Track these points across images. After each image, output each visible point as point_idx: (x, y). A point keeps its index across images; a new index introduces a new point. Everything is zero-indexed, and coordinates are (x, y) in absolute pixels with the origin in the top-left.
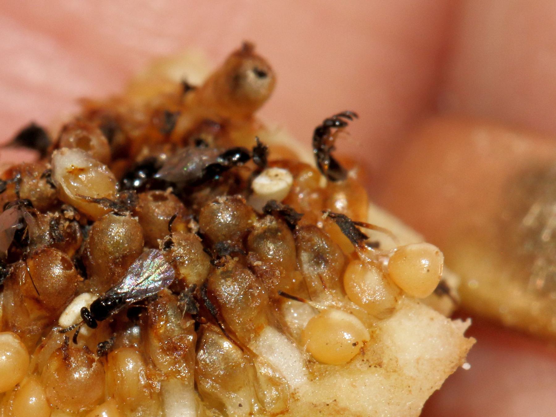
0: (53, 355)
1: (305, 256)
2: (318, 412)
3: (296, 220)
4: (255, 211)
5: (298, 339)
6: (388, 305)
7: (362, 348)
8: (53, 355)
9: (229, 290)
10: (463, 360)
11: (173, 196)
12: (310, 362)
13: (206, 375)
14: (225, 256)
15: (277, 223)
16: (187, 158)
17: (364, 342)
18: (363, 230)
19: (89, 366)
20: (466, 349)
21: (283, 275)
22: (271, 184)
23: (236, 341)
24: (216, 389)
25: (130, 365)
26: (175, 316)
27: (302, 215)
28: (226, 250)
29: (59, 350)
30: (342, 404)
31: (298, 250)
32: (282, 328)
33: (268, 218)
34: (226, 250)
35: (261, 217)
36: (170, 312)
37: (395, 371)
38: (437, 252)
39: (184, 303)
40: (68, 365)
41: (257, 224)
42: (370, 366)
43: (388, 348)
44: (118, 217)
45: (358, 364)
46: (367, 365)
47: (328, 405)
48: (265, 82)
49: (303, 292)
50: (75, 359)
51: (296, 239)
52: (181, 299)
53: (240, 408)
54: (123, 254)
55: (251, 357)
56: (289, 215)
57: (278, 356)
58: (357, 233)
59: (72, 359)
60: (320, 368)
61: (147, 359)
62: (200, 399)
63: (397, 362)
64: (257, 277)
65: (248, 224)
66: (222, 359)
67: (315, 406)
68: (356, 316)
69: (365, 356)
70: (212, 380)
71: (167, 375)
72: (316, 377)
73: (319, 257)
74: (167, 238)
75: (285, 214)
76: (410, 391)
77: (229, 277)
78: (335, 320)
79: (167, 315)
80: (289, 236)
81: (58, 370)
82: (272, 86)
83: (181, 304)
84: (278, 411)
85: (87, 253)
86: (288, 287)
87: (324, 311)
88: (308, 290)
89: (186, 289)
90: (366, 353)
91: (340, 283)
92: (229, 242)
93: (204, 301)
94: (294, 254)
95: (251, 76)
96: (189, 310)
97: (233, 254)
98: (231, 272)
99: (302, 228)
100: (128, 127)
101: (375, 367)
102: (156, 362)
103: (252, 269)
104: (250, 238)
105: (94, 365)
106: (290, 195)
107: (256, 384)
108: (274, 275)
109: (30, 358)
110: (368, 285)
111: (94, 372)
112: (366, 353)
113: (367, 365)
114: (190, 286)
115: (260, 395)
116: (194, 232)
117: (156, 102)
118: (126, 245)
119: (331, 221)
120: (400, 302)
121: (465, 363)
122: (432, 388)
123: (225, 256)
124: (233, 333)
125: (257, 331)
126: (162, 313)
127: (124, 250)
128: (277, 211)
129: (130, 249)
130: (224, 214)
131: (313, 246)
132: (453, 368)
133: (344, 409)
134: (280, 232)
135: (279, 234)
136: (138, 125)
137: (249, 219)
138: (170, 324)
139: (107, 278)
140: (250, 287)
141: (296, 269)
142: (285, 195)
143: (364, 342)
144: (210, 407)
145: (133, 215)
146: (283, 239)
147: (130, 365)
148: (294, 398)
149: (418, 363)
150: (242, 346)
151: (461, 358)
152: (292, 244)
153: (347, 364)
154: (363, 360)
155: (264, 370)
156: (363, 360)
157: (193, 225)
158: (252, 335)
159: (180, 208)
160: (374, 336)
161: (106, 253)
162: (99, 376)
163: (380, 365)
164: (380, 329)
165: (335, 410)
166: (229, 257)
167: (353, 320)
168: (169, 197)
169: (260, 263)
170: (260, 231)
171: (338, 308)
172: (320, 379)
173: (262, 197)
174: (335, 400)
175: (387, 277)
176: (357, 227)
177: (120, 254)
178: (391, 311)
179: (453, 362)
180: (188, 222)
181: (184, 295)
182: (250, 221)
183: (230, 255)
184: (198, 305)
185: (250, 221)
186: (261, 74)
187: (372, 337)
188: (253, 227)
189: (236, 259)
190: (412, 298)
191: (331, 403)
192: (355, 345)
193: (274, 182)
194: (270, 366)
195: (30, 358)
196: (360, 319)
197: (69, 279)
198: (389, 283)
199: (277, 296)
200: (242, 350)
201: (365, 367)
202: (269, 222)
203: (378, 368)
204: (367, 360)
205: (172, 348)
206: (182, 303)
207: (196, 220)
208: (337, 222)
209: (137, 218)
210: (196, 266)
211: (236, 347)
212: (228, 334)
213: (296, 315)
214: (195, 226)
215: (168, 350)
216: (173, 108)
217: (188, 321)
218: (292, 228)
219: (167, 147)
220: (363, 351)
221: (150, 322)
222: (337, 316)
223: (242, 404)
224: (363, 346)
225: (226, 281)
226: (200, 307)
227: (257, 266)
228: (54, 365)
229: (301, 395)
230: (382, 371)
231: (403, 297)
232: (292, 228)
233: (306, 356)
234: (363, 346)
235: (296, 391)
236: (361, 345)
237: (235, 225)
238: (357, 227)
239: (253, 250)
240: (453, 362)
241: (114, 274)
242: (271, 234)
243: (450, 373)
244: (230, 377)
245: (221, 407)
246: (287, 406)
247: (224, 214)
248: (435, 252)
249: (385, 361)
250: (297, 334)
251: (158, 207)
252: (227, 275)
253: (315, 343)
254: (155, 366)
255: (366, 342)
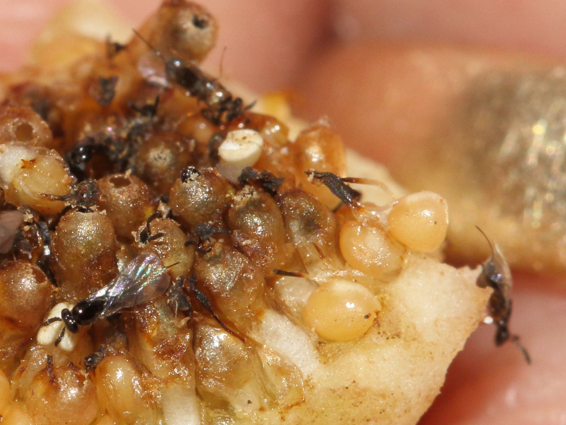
0: (36, 378)
1: (295, 226)
2: (338, 397)
3: (278, 187)
4: (230, 183)
5: (300, 320)
6: (394, 267)
7: (375, 319)
8: (36, 378)
9: (215, 275)
10: (484, 314)
11: (135, 177)
12: (321, 343)
13: (205, 375)
14: (208, 239)
15: (259, 193)
16: (124, 126)
17: (377, 313)
18: (354, 186)
19: (80, 385)
20: (484, 301)
21: (276, 251)
22: (239, 148)
23: (235, 332)
24: (220, 388)
25: (120, 373)
26: (167, 315)
27: (282, 180)
28: (208, 232)
29: (43, 371)
30: (363, 384)
31: (285, 220)
32: (279, 307)
33: (247, 189)
34: (208, 232)
35: (238, 188)
36: (159, 313)
37: (414, 339)
38: (441, 201)
39: (174, 299)
40: (57, 388)
41: (237, 198)
42: (388, 338)
43: (402, 314)
44: (85, 214)
45: (373, 337)
46: (384, 337)
47: (347, 388)
48: (207, 31)
49: (297, 267)
50: (62, 379)
51: (281, 208)
52: (171, 296)
53: (245, 403)
54: (97, 255)
55: (254, 347)
56: (270, 182)
57: (282, 340)
58: (347, 194)
59: (60, 380)
60: (332, 347)
61: (140, 368)
62: (199, 400)
63: (414, 328)
64: (249, 258)
65: (226, 198)
66: (222, 354)
67: (334, 391)
68: (361, 284)
69: (381, 328)
70: (215, 379)
71: (166, 382)
72: (329, 358)
73: (310, 225)
74: (142, 228)
75: (262, 180)
76: (432, 358)
77: (219, 262)
78: (339, 293)
79: (157, 315)
80: (275, 206)
81: (46, 395)
82: (214, 34)
83: (170, 302)
84: (293, 402)
85: (55, 259)
86: (283, 264)
87: (325, 284)
88: (302, 261)
89: (174, 284)
90: (379, 322)
91: (335, 249)
92: (210, 222)
93: (196, 293)
94: (282, 224)
95: (188, 25)
96: (180, 306)
97: (217, 236)
98: (219, 257)
99: (286, 194)
100: (60, 103)
101: (393, 338)
102: (151, 369)
103: (240, 249)
104: (231, 214)
105: (85, 383)
106: (262, 159)
107: (262, 376)
108: (267, 253)
109: (10, 384)
110: (365, 244)
111: (87, 390)
112: (379, 322)
113: (384, 337)
114: (177, 279)
115: (268, 386)
116: (164, 216)
117: (85, 69)
118: (100, 244)
119: (318, 182)
120: (406, 261)
121: (485, 317)
122: (454, 350)
123: (208, 239)
124: (232, 324)
125: (257, 316)
126: (151, 315)
127: (99, 250)
128: (257, 180)
129: (104, 248)
130: (197, 191)
131: (302, 212)
132: (474, 324)
133: (365, 390)
134: (264, 203)
135: (263, 205)
136: (70, 99)
137: (226, 193)
138: (160, 323)
139: (82, 283)
140: (244, 271)
141: (286, 241)
142: (257, 158)
143: (377, 313)
144: (213, 408)
145: (100, 209)
146: (268, 210)
147: (120, 373)
148: (308, 385)
149: (436, 325)
150: (241, 337)
151: (480, 312)
152: (278, 214)
153: (359, 338)
154: (379, 333)
155: (268, 359)
156: (379, 333)
157: (163, 208)
158: (254, 323)
159: (146, 191)
160: (385, 302)
161: (78, 256)
162: (90, 395)
163: (398, 335)
164: (390, 294)
165: (356, 393)
166: (213, 240)
167: (358, 288)
168: (131, 180)
169: (249, 242)
170: (242, 205)
171: (341, 278)
172: (334, 361)
173: (233, 165)
174: (354, 381)
175: (389, 237)
176: (346, 183)
177: (94, 256)
178: (398, 272)
179: (472, 318)
180: (156, 205)
181: (173, 291)
182: (227, 195)
183: (213, 237)
184: (188, 298)
185: (227, 195)
186: (199, 23)
187: (383, 305)
188: (233, 201)
189: (221, 241)
190: (417, 253)
191: (350, 385)
192: (367, 317)
193: (244, 146)
194: (275, 353)
195: (10, 384)
196: (366, 286)
197: (45, 292)
198: (392, 243)
199: (272, 273)
200: (243, 340)
201: (382, 340)
202: (248, 194)
203: (397, 339)
204: (384, 332)
205: (168, 351)
206: (172, 300)
207: (166, 201)
208: (324, 182)
209: (104, 212)
210: (180, 255)
211: (237, 339)
212: (224, 324)
213: (292, 291)
214: (165, 208)
215: (164, 353)
216: (105, 73)
217: (183, 319)
218: (274, 194)
219: (111, 119)
220: (377, 323)
221: (138, 326)
222: (342, 287)
223: (252, 401)
224: (376, 317)
225: (217, 268)
226: (191, 301)
227: (246, 245)
228: (40, 388)
229: (315, 381)
230: (402, 341)
231: (409, 253)
232: (274, 194)
233: (315, 338)
234: (376, 317)
235: (310, 378)
236: (374, 316)
237: (212, 202)
238: (346, 183)
239: (237, 228)
240: (472, 318)
241: (91, 277)
242: (254, 207)
243: (472, 331)
244: (234, 372)
245: (224, 405)
246: (302, 396)
247: (197, 191)
248: (438, 201)
249: (403, 330)
250: (298, 312)
251: (121, 193)
252: (215, 260)
253: (321, 321)
254: (150, 373)
255: (379, 312)
